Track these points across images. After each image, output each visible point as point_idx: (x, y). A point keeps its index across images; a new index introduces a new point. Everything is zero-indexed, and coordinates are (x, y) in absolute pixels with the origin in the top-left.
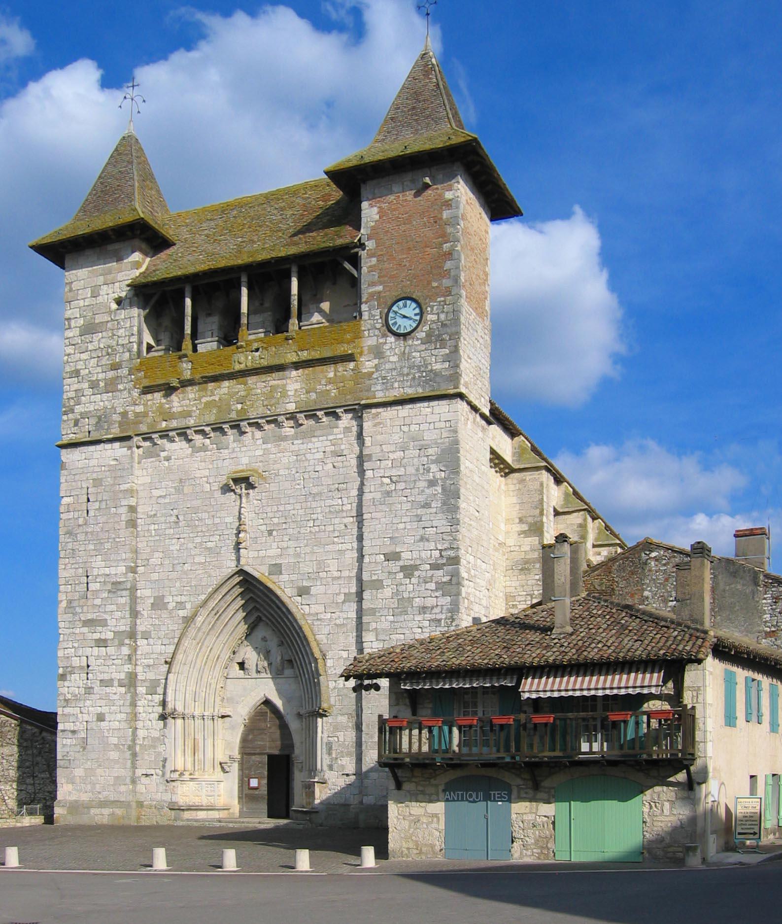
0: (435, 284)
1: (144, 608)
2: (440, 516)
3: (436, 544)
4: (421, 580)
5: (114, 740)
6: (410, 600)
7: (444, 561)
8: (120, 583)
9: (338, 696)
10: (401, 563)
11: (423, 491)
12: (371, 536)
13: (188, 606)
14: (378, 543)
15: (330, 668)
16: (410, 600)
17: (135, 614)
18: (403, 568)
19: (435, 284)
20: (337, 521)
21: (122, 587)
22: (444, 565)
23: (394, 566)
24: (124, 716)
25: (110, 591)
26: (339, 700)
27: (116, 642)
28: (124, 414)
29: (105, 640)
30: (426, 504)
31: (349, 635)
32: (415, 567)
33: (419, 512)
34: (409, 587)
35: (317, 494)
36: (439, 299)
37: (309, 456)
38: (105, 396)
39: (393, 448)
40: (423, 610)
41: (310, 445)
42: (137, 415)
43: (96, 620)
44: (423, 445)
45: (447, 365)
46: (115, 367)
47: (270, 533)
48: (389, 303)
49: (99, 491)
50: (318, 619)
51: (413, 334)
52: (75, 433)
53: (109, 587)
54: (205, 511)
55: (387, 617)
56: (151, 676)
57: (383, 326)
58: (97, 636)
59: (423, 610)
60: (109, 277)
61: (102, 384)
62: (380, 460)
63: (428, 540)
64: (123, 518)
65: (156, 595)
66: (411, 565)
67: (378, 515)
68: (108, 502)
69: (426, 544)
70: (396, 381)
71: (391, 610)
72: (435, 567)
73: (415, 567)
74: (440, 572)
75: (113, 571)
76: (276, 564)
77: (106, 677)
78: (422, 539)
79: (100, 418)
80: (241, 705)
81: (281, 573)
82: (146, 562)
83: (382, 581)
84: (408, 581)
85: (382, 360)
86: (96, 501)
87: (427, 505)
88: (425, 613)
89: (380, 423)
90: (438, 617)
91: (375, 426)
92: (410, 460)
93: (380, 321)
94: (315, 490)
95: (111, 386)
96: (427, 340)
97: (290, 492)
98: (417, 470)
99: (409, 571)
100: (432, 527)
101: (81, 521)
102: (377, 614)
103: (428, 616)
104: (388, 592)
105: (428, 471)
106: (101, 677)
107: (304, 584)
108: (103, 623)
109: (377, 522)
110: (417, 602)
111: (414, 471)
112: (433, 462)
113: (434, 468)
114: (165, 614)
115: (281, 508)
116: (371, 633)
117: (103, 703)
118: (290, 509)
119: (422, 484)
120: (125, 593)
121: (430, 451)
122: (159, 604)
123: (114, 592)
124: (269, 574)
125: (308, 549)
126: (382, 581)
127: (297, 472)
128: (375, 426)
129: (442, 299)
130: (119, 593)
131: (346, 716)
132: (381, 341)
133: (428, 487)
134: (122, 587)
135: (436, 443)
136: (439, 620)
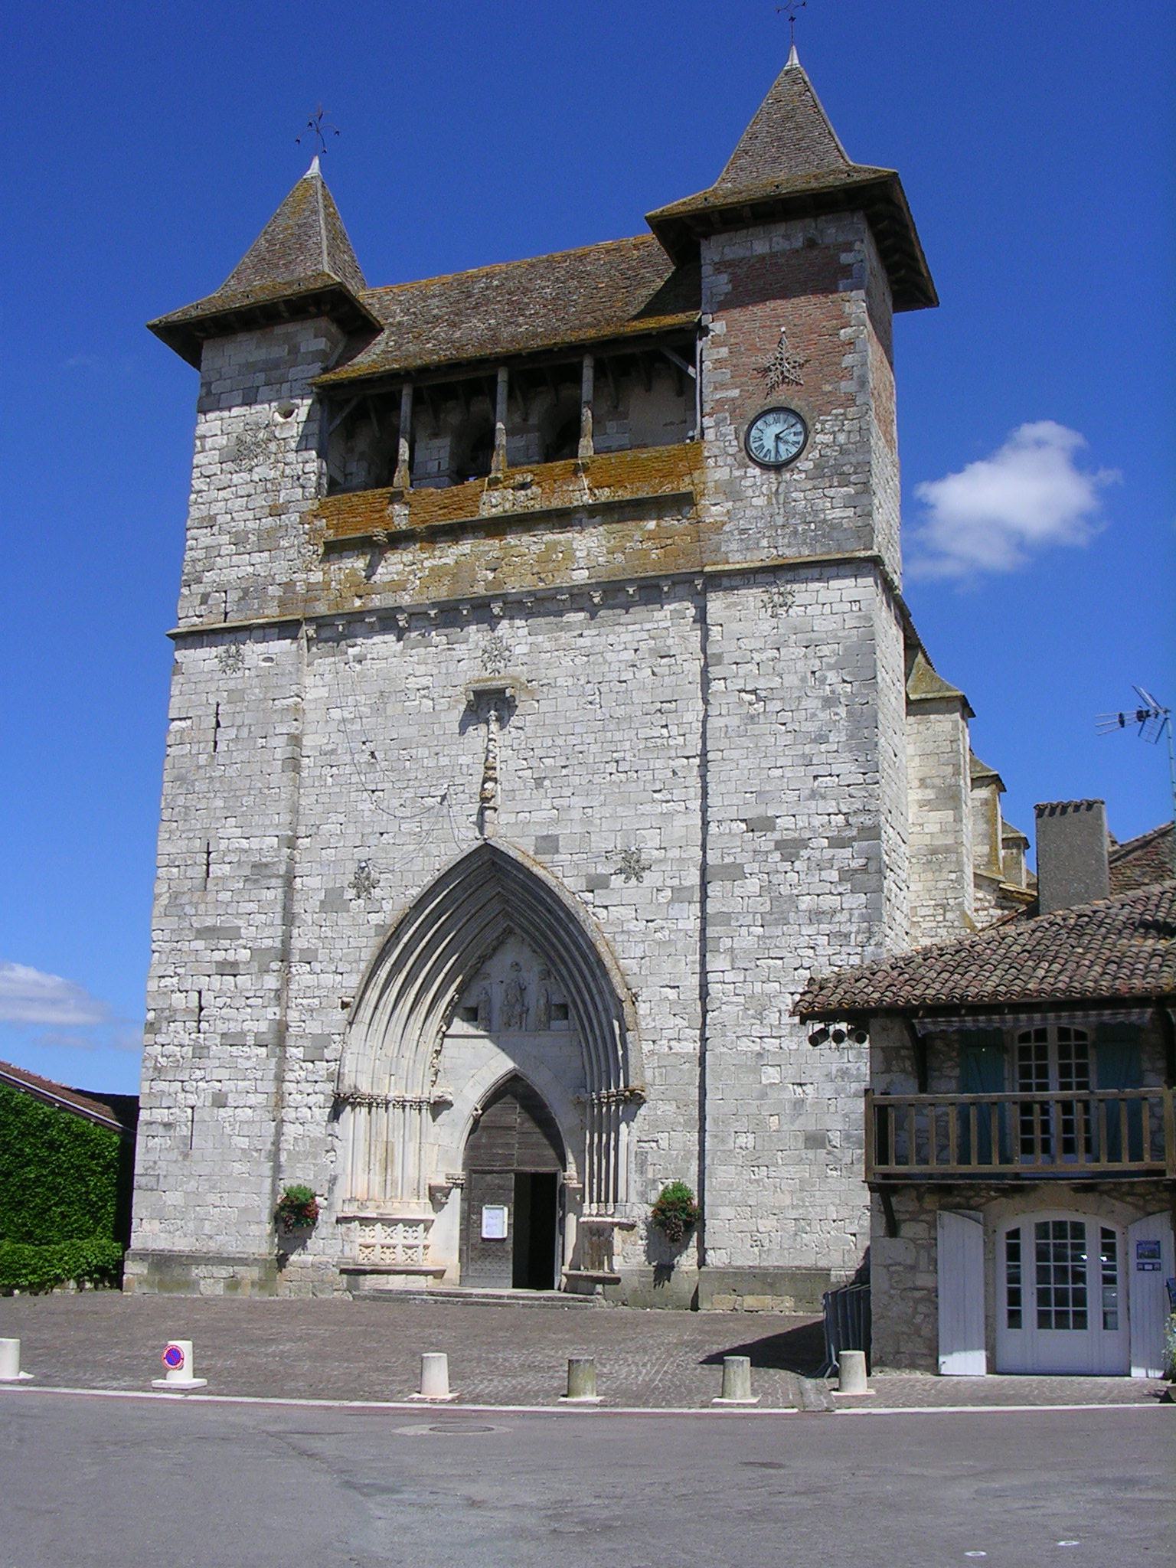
0: (828, 388)
1: (307, 907)
2: (846, 756)
3: (838, 804)
4: (813, 865)
5: (243, 1143)
6: (794, 899)
7: (855, 833)
8: (266, 865)
9: (659, 1067)
10: (777, 836)
11: (814, 715)
12: (722, 788)
13: (387, 906)
14: (735, 802)
15: (645, 1017)
16: (794, 899)
17: (289, 918)
18: (779, 845)
19: (828, 388)
20: (659, 764)
21: (268, 872)
22: (854, 839)
23: (766, 841)
24: (261, 1098)
25: (247, 879)
26: (661, 1075)
27: (255, 965)
28: (289, 586)
29: (235, 964)
30: (821, 736)
31: (679, 960)
32: (803, 843)
33: (807, 749)
34: (790, 878)
35: (624, 719)
36: (834, 412)
37: (609, 656)
38: (256, 557)
39: (759, 644)
40: (816, 916)
41: (612, 639)
42: (310, 586)
43: (221, 928)
44: (811, 640)
45: (850, 512)
46: (276, 511)
47: (539, 782)
48: (752, 416)
49: (238, 709)
50: (623, 932)
51: (792, 466)
52: (201, 616)
53: (247, 871)
54: (424, 745)
55: (752, 929)
56: (314, 1027)
57: (740, 450)
58: (219, 956)
59: (816, 916)
60: (276, 374)
61: (253, 538)
62: (737, 664)
63: (824, 798)
64: (279, 754)
65: (330, 885)
66: (794, 840)
67: (735, 754)
68: (253, 729)
69: (821, 803)
70: (764, 537)
71: (758, 916)
72: (837, 843)
73: (803, 843)
74: (847, 852)
75: (255, 844)
76: (548, 836)
77: (234, 1027)
78: (813, 795)
79: (246, 591)
80: (471, 1083)
81: (557, 852)
82: (314, 829)
83: (741, 866)
84: (787, 866)
85: (738, 504)
86: (233, 726)
87: (821, 739)
88: (819, 922)
89: (736, 604)
90: (845, 929)
91: (728, 607)
92: (790, 663)
93: (735, 443)
94: (620, 712)
95: (268, 542)
96: (819, 472)
97: (577, 714)
98: (803, 680)
99: (790, 849)
100: (830, 775)
101: (203, 759)
102: (733, 923)
103: (825, 928)
104: (752, 885)
105: (823, 681)
106: (222, 1027)
107: (598, 871)
108: (234, 934)
109: (733, 765)
110: (805, 903)
111: (797, 682)
112: (830, 667)
113: (832, 677)
114: (343, 919)
115: (560, 741)
116: (723, 956)
117: (223, 1074)
118: (575, 742)
119: (812, 704)
120: (274, 882)
121: (825, 650)
122: (333, 902)
123: (256, 881)
124: (536, 854)
125: (607, 811)
126: (741, 866)
127: (589, 682)
128: (728, 607)
129: (841, 411)
130: (264, 882)
131: (674, 1102)
132: (737, 473)
133: (824, 708)
134: (268, 872)
135: (836, 636)
136: (847, 936)
